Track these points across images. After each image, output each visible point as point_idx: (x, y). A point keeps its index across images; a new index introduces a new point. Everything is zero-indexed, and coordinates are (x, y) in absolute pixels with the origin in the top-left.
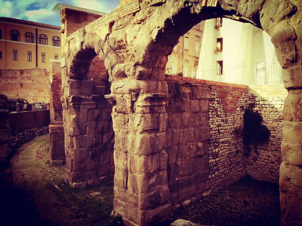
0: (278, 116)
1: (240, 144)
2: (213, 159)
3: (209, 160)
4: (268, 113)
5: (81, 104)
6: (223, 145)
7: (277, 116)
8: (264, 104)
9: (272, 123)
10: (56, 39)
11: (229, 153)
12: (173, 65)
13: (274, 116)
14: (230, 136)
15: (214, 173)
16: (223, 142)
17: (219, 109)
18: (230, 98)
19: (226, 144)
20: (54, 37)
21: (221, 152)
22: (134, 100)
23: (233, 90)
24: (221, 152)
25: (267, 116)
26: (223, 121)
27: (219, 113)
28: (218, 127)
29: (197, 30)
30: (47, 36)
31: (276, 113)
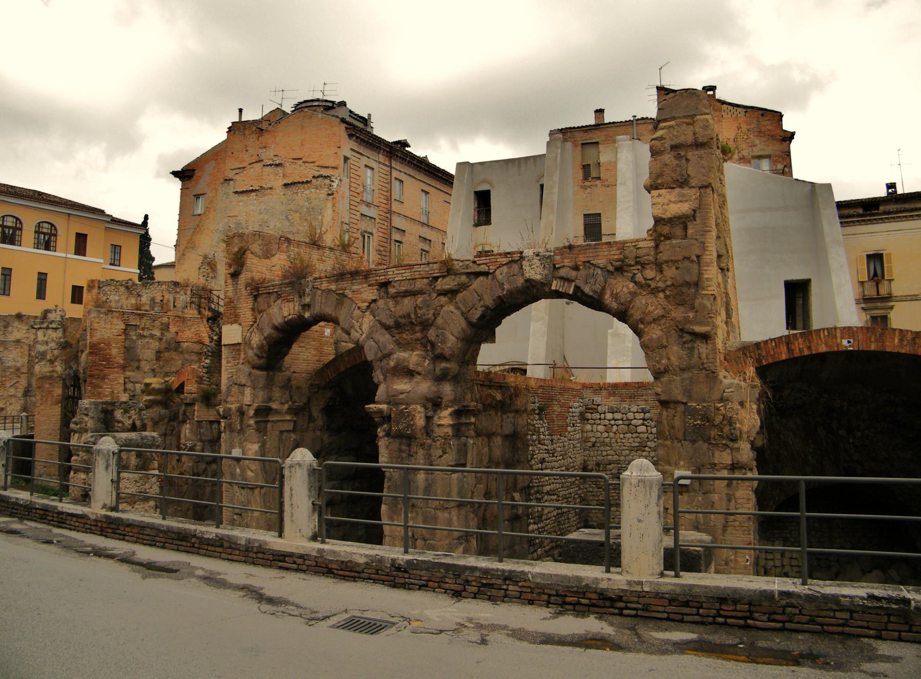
0: (638, 440)
1: (574, 498)
2: (534, 523)
3: (529, 525)
4: (622, 436)
5: (268, 421)
6: (550, 497)
7: (636, 440)
8: (613, 419)
9: (628, 455)
10: (9, 224)
11: (558, 514)
12: (489, 356)
13: (631, 440)
14: (559, 481)
15: (536, 551)
16: (548, 493)
17: (542, 430)
18: (557, 408)
19: (552, 497)
20: (3, 217)
21: (546, 511)
22: (430, 414)
23: (561, 394)
24: (546, 511)
25: (619, 440)
26: (547, 451)
27: (542, 437)
28: (541, 463)
29: (423, 224)
30: (23, 220)
31: (634, 435)
